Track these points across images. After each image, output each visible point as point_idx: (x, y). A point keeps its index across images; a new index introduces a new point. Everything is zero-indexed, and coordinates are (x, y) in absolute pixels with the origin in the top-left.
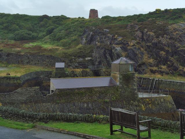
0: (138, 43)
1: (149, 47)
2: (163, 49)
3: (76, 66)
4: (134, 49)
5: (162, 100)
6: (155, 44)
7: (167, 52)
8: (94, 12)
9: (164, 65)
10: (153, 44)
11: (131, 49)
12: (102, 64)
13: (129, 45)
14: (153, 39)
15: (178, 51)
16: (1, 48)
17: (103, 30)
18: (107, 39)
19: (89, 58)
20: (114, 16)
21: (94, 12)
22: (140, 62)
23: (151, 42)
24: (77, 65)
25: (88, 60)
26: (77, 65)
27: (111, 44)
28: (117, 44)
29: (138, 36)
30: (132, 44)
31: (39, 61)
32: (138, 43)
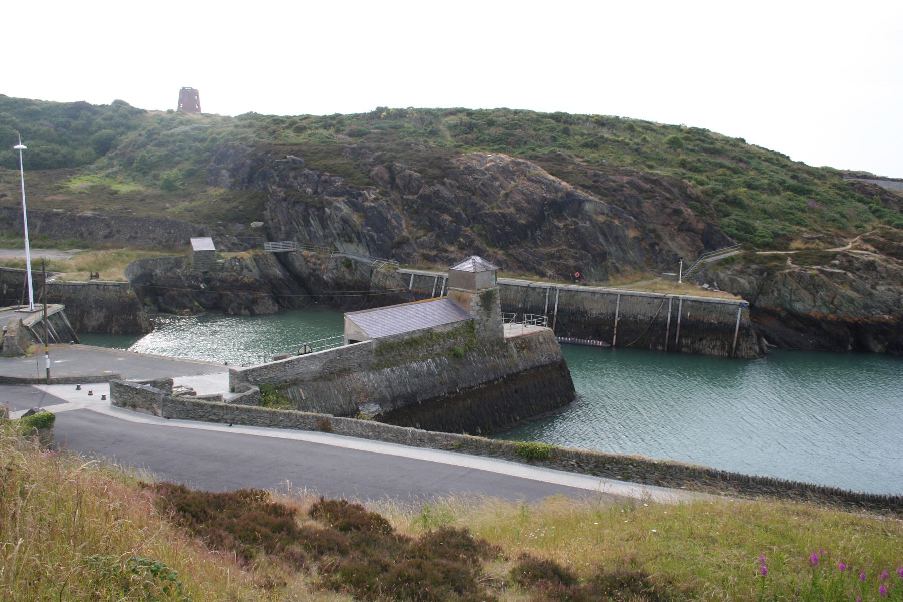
0: (384, 194)
1: (409, 204)
2: (446, 210)
3: (234, 244)
4: (380, 209)
5: (541, 340)
6: (426, 198)
7: (457, 218)
8: (189, 97)
9: (452, 243)
10: (421, 197)
11: (374, 207)
12: (295, 239)
13: (366, 199)
14: (420, 188)
15: (480, 215)
16: (203, 244)
17: (286, 157)
18: (301, 180)
19: (261, 224)
20: (100, 96)
21: (189, 97)
22: (397, 239)
23: (416, 193)
24: (235, 240)
25: (257, 229)
26: (235, 240)
27: (315, 192)
28: (335, 194)
29: (382, 178)
30: (373, 196)
31: (137, 233)
32: (384, 194)
